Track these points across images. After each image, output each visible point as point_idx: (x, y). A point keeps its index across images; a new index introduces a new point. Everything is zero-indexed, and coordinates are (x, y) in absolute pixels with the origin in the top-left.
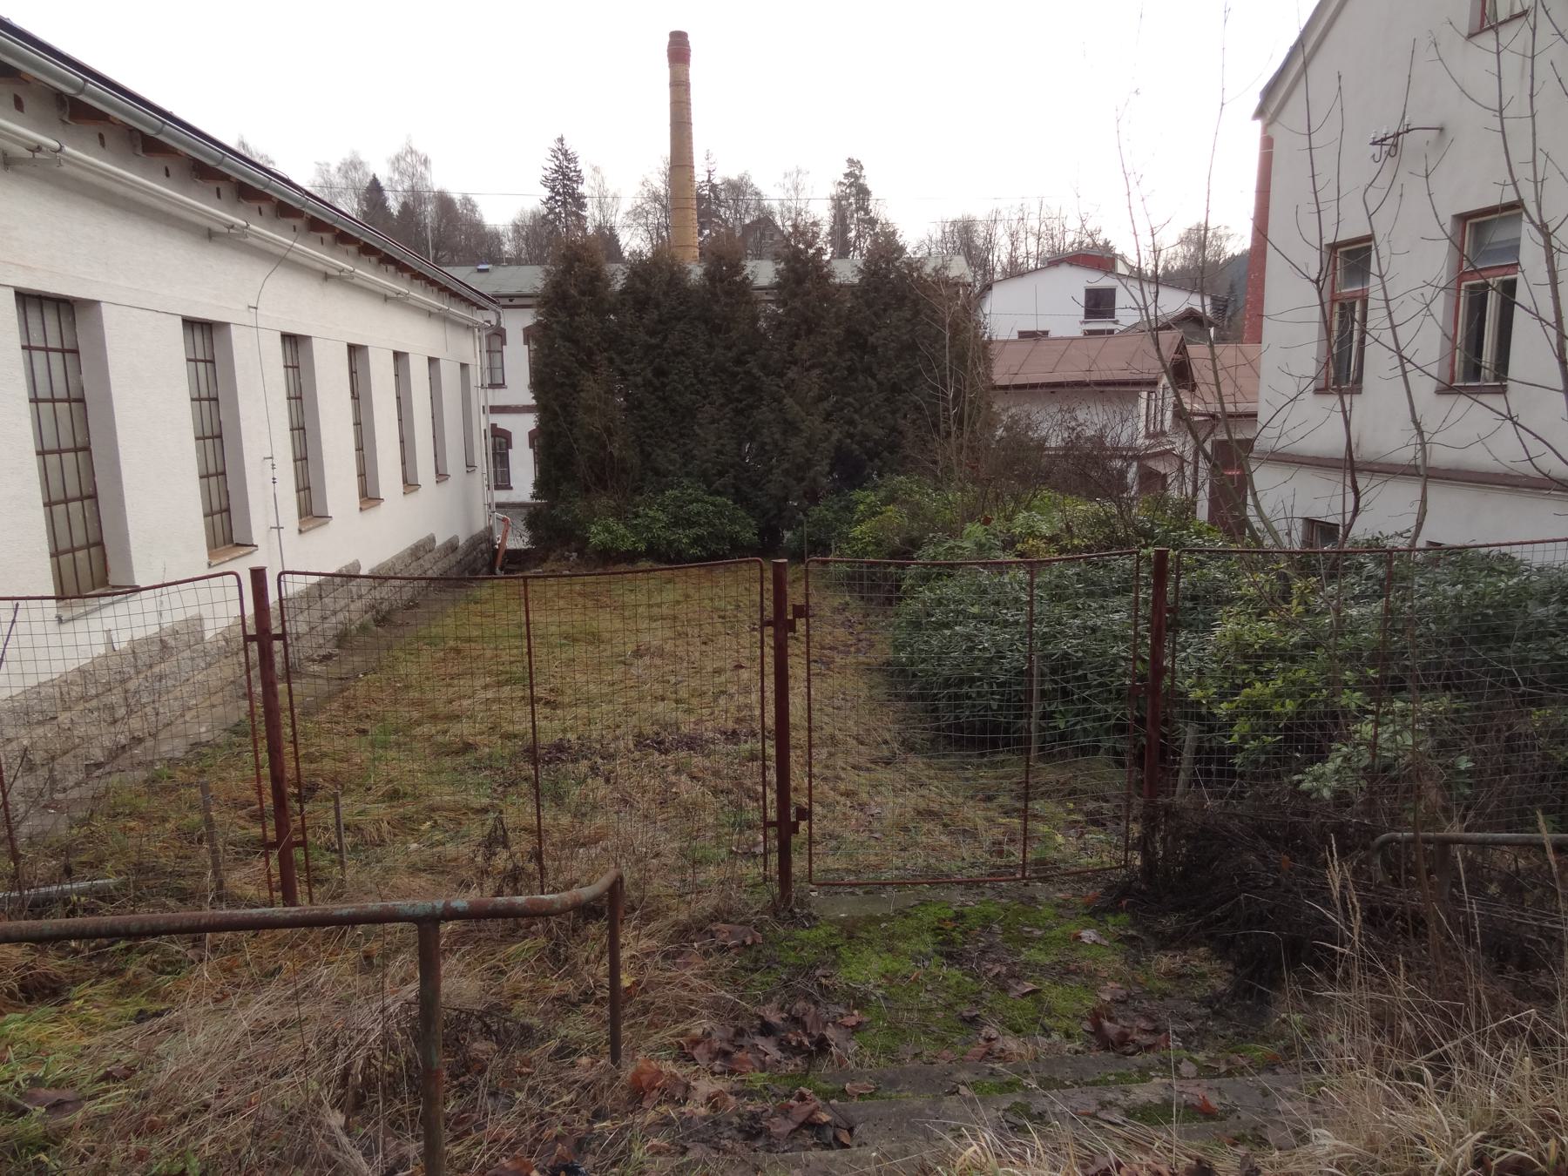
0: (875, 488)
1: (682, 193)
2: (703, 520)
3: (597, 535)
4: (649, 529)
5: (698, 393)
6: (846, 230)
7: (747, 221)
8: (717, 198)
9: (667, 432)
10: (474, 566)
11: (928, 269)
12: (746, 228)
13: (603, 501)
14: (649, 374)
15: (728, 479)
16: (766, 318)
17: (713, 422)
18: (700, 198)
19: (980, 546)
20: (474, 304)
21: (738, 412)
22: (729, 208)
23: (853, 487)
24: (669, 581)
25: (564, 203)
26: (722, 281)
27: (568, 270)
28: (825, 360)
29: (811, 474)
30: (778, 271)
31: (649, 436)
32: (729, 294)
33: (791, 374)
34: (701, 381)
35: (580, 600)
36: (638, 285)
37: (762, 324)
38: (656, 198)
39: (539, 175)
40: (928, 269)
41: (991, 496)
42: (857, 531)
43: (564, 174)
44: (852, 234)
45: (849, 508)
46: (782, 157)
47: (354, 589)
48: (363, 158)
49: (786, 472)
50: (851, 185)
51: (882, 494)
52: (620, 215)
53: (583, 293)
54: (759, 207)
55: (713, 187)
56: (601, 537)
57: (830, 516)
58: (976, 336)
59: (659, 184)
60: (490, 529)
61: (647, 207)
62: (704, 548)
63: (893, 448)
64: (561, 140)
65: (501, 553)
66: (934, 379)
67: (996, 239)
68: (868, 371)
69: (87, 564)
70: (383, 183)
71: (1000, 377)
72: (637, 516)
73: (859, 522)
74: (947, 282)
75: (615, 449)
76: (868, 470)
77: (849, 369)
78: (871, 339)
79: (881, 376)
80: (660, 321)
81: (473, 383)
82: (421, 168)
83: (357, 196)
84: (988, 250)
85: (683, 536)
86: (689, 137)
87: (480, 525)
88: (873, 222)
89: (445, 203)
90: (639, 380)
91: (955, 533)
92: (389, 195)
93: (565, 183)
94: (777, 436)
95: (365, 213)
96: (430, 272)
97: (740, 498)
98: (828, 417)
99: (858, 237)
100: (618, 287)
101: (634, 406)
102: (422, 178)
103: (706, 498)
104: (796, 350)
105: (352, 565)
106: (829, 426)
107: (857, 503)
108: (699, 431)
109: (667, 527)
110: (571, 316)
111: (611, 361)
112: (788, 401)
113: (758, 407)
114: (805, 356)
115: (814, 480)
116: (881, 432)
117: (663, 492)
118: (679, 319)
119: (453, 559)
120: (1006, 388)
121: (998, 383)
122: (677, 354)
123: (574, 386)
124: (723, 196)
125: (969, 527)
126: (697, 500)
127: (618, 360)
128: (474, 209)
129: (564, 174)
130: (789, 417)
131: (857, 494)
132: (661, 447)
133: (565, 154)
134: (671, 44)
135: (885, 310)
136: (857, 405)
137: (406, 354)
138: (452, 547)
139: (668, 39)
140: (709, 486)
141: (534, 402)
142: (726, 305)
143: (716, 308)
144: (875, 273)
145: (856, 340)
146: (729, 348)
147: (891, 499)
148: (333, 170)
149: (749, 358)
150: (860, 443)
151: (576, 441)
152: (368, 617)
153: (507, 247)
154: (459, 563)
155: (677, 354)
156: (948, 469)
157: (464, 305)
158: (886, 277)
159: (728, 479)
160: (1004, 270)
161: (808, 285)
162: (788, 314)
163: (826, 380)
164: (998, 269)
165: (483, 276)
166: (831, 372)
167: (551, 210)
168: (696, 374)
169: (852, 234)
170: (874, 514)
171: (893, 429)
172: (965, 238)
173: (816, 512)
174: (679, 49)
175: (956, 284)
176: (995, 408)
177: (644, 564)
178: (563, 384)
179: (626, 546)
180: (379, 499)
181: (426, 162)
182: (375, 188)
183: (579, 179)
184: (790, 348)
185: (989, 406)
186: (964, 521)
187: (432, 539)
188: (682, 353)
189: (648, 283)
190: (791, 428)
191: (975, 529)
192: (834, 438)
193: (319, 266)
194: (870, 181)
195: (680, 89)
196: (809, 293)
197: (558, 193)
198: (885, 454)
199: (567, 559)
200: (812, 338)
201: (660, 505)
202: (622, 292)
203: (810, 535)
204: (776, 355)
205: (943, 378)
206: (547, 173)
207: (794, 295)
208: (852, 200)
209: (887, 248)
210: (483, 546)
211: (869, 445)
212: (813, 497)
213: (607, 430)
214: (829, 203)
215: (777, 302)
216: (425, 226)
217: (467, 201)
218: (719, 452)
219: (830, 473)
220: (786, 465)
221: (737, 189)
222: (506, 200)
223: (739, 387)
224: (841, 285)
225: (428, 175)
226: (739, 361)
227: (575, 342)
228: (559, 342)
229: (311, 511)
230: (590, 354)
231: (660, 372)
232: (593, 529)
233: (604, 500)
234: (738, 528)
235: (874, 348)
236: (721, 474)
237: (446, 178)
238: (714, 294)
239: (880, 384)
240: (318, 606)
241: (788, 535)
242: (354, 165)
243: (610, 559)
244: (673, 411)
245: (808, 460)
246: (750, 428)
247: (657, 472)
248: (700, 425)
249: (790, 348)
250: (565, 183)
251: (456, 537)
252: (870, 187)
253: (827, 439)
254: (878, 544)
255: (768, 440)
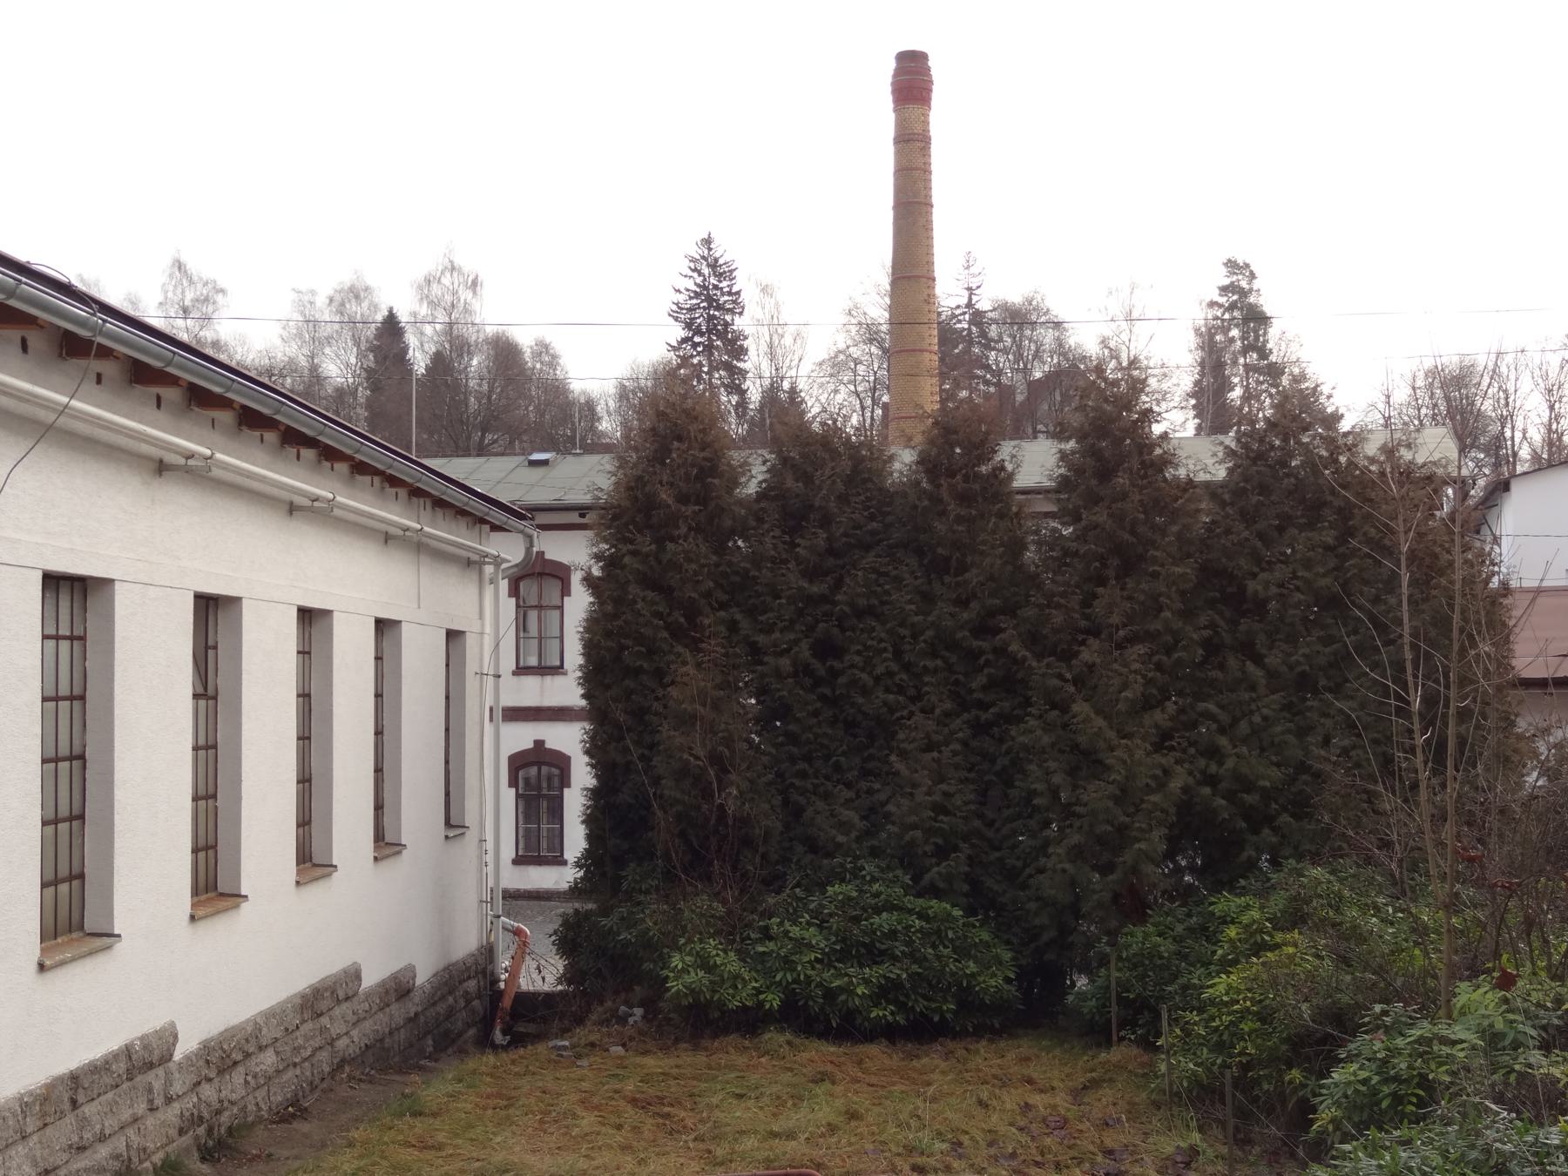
0: (1264, 893)
1: (914, 325)
2: (900, 948)
3: (683, 974)
4: (788, 963)
5: (901, 690)
6: (1224, 386)
7: (1038, 375)
8: (983, 334)
9: (837, 767)
10: (459, 1020)
11: (1371, 448)
12: (1033, 386)
13: (701, 904)
14: (804, 651)
15: (957, 864)
16: (1039, 543)
17: (929, 748)
18: (948, 335)
19: (1493, 1039)
20: (482, 521)
21: (980, 728)
22: (1006, 351)
23: (1217, 888)
24: (820, 1078)
25: (709, 348)
26: (952, 474)
27: (659, 456)
28: (1157, 626)
29: (1128, 857)
30: (1063, 456)
31: (803, 775)
32: (964, 498)
33: (1086, 655)
34: (907, 667)
35: (630, 1114)
36: (790, 483)
37: (1030, 555)
38: (870, 334)
39: (668, 300)
40: (1371, 448)
41: (1514, 919)
42: (1220, 985)
43: (709, 299)
44: (1237, 393)
45: (1207, 931)
46: (1103, 263)
47: (157, 1086)
48: (370, 281)
49: (1077, 853)
50: (1232, 307)
51: (1277, 902)
52: (805, 368)
53: (683, 499)
54: (1060, 348)
55: (978, 317)
56: (690, 978)
57: (1167, 947)
58: (1469, 581)
59: (878, 311)
60: (488, 952)
61: (855, 352)
62: (902, 1006)
63: (1301, 808)
64: (707, 242)
65: (507, 1002)
66: (1375, 666)
67: (1518, 401)
68: (1248, 650)
69: (72, 916)
70: (403, 317)
71: (1528, 660)
72: (767, 935)
73: (1226, 966)
74: (1406, 475)
75: (730, 798)
76: (1249, 852)
77: (1207, 644)
78: (1252, 586)
79: (1273, 660)
80: (831, 552)
81: (471, 667)
82: (465, 295)
83: (357, 343)
84: (1503, 420)
85: (859, 981)
86: (928, 228)
87: (466, 943)
88: (1275, 371)
89: (504, 353)
90: (785, 663)
91: (1432, 1002)
92: (411, 339)
93: (711, 315)
94: (1057, 779)
95: (369, 371)
96: (401, 469)
97: (979, 902)
98: (1162, 741)
99: (1248, 397)
100: (751, 488)
101: (774, 712)
102: (467, 310)
103: (910, 901)
104: (1099, 607)
105: (159, 1034)
106: (1166, 760)
107: (1225, 921)
108: (900, 766)
109: (826, 961)
110: (660, 542)
111: (733, 626)
112: (1080, 708)
113: (1020, 720)
114: (1115, 619)
115: (1135, 870)
116: (1276, 774)
117: (822, 887)
118: (867, 548)
119: (398, 1012)
120: (1541, 683)
121: (1526, 674)
122: (860, 614)
123: (659, 674)
124: (993, 331)
125: (1465, 993)
126: (890, 907)
127: (745, 625)
128: (553, 361)
129: (709, 299)
130: (1082, 740)
131: (1225, 903)
132: (826, 796)
133: (714, 265)
134: (898, 72)
135: (1281, 529)
136: (1225, 718)
137: (326, 614)
138: (399, 988)
139: (891, 65)
140: (916, 878)
141: (583, 703)
142: (959, 519)
143: (940, 527)
144: (1259, 457)
145: (1222, 587)
146: (963, 603)
147: (1295, 918)
148: (321, 301)
149: (1004, 621)
150: (1230, 796)
151: (656, 781)
152: (187, 1140)
153: (605, 425)
154: (412, 1020)
155: (860, 614)
156: (1415, 864)
157: (462, 523)
158: (1284, 464)
159: (957, 864)
160: (1536, 457)
161: (1122, 480)
162: (1080, 537)
163: (1159, 667)
164: (1525, 453)
165: (540, 471)
166: (1168, 652)
167: (685, 360)
168: (898, 654)
169: (1237, 393)
170: (1259, 949)
171: (1302, 768)
172: (1457, 400)
173: (1137, 938)
174: (912, 81)
175: (1428, 482)
176: (1522, 725)
177: (775, 1038)
178: (638, 671)
179: (739, 998)
180: (237, 897)
181: (474, 285)
182: (391, 327)
183: (737, 307)
184: (1087, 603)
185: (1508, 722)
186: (1454, 975)
187: (354, 975)
188: (870, 611)
189: (807, 479)
190: (1086, 762)
191: (1477, 997)
192: (1175, 785)
193: (145, 448)
194: (1267, 302)
195: (912, 148)
196: (1124, 496)
197: (698, 332)
198: (1285, 818)
199: (623, 1020)
200: (1130, 584)
201: (816, 914)
202: (761, 496)
203: (1124, 986)
204: (1058, 618)
205: (1399, 667)
206: (681, 298)
207: (1094, 500)
208: (1235, 333)
209: (1300, 411)
210: (472, 985)
211: (1251, 799)
212: (1133, 905)
213: (715, 759)
214: (1192, 340)
215: (1062, 515)
216: (467, 393)
217: (543, 348)
218: (939, 809)
219: (1170, 855)
220: (1076, 839)
221: (1018, 318)
222: (607, 349)
223: (980, 680)
224: (1190, 483)
225: (476, 305)
226: (984, 629)
227: (666, 591)
228: (634, 590)
229: (213, 887)
230: (692, 613)
231: (827, 649)
232: (676, 961)
233: (703, 902)
234: (972, 967)
235: (1260, 606)
236: (942, 853)
237: (510, 311)
238: (935, 499)
239: (1272, 674)
240: (70, 1119)
241: (1082, 982)
242: (356, 293)
243: (706, 1022)
244: (850, 726)
245: (1122, 829)
246: (1003, 762)
247: (813, 847)
248: (903, 754)
249: (1087, 603)
250: (711, 315)
251: (410, 970)
252: (1268, 310)
253: (1162, 786)
254: (1264, 1017)
255: (1039, 786)
